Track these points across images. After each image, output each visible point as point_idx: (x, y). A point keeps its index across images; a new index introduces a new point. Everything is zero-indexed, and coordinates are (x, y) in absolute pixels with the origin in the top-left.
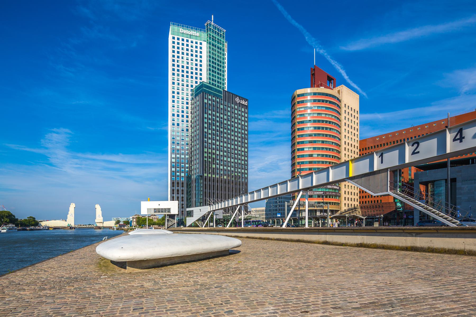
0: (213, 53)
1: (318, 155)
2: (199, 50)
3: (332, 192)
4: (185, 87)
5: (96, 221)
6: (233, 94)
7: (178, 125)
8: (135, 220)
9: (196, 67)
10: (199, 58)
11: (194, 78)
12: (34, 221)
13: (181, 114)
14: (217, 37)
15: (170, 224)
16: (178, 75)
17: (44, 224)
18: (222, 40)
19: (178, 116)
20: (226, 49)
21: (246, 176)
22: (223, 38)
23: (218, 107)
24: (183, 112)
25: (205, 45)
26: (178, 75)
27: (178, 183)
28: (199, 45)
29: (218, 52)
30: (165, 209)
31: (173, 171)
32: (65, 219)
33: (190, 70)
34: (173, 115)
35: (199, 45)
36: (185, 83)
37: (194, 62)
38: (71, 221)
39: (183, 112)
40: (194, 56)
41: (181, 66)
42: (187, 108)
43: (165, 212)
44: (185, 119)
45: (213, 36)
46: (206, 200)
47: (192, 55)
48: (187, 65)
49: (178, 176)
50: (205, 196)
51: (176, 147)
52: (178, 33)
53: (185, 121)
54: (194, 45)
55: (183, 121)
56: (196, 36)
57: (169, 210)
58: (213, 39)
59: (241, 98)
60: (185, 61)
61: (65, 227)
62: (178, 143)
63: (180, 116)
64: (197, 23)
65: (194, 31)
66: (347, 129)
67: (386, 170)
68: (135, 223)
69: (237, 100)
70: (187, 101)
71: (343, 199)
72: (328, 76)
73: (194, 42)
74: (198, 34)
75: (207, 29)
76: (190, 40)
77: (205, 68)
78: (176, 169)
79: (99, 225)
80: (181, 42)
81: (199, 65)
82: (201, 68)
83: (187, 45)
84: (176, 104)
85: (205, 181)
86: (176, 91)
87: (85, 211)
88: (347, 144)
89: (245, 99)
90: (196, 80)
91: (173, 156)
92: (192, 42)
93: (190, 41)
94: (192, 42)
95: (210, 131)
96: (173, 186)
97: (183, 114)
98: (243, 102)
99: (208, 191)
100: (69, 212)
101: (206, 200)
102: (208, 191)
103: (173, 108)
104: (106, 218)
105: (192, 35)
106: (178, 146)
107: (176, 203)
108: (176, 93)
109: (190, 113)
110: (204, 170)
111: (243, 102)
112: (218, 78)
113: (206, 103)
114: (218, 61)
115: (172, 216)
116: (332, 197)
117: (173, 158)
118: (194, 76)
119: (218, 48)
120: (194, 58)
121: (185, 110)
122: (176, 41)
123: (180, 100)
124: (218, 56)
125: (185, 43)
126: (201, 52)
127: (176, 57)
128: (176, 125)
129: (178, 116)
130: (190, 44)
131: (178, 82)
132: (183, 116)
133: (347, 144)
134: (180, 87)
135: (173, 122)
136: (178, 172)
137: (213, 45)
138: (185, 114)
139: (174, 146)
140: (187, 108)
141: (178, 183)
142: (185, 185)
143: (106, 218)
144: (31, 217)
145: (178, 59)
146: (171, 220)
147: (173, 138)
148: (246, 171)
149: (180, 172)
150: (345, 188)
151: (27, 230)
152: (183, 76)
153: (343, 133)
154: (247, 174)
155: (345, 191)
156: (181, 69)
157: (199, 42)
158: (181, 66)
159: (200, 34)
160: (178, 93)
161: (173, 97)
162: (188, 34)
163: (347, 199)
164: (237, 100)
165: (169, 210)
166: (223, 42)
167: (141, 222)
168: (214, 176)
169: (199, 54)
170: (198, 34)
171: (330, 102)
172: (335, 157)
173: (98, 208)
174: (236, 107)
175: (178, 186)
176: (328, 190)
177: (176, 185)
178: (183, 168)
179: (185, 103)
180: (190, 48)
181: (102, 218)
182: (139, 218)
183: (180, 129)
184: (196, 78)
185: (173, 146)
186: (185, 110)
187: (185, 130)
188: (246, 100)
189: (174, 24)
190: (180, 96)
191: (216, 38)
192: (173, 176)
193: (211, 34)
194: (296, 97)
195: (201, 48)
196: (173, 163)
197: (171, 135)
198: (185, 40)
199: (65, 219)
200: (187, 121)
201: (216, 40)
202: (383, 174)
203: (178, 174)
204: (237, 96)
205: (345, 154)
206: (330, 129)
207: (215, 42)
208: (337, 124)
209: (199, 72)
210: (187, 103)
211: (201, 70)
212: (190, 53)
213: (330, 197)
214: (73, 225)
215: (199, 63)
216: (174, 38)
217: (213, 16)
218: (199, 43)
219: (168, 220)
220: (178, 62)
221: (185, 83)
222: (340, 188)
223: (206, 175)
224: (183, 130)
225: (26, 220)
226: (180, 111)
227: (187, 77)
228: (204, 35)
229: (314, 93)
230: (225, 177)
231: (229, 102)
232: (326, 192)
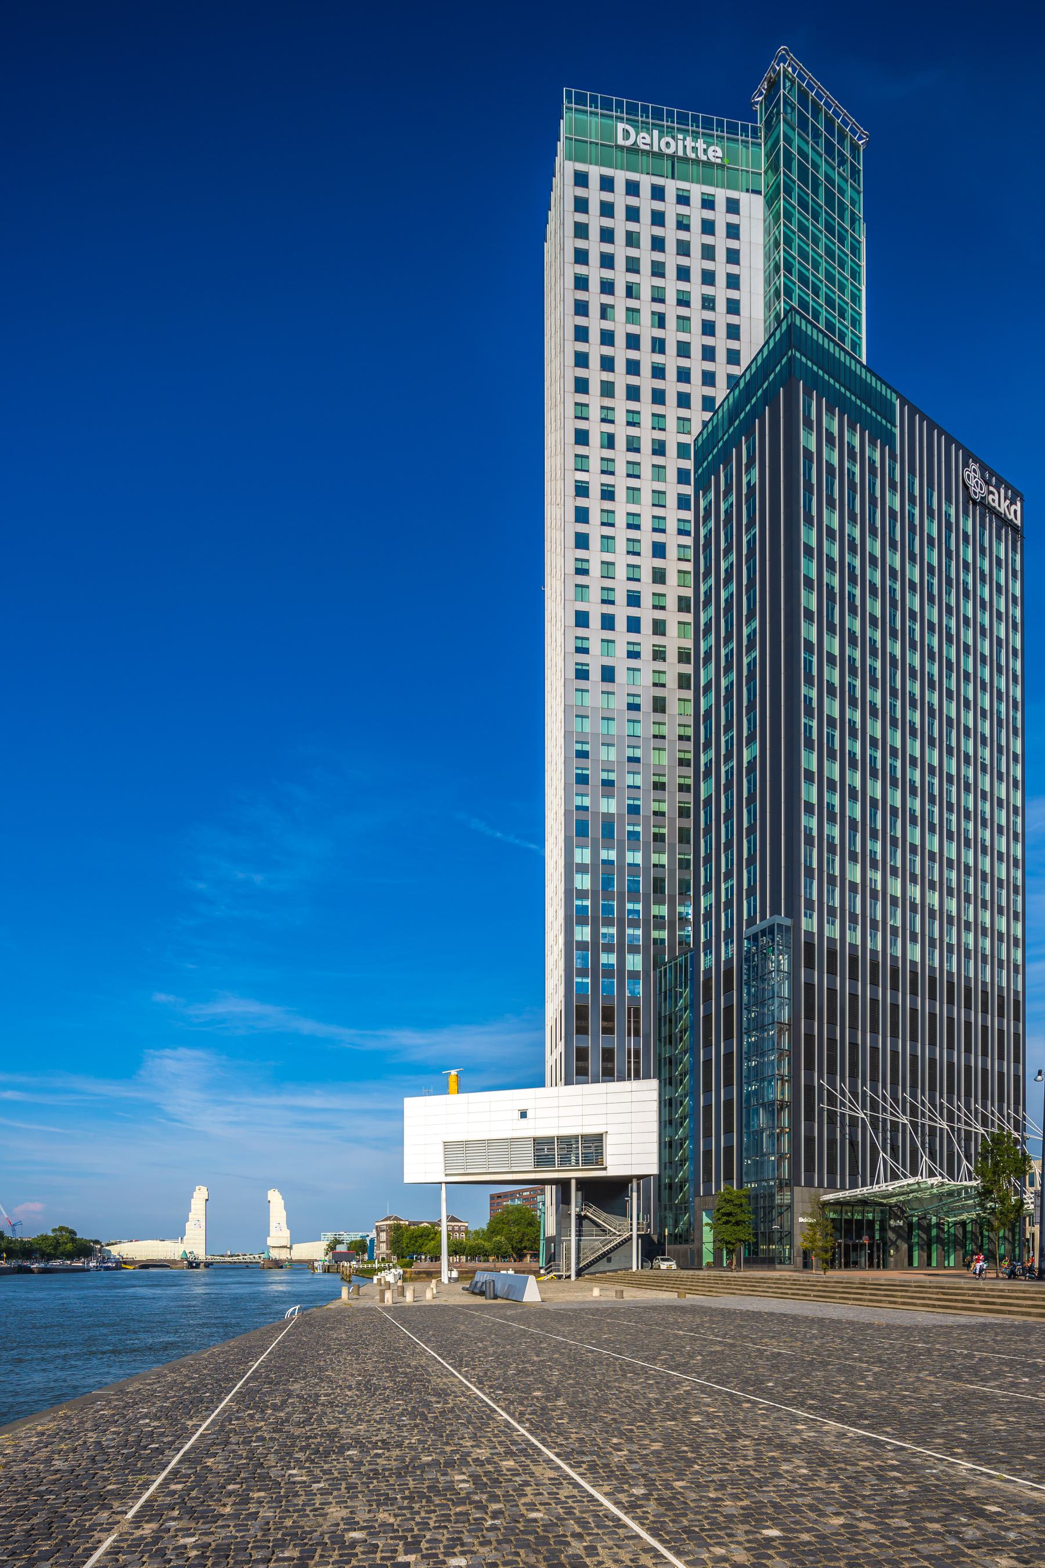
2: (721, 242)
4: (646, 459)
5: (270, 1242)
7: (608, 674)
8: (383, 1236)
9: (709, 341)
10: (721, 293)
12: (73, 1240)
13: (621, 612)
15: (595, 1244)
16: (607, 389)
17: (115, 1251)
19: (608, 622)
24: (634, 599)
26: (607, 389)
27: (608, 1014)
28: (721, 217)
30: (567, 1142)
31: (582, 946)
32: (178, 1233)
33: (671, 361)
34: (582, 619)
35: (721, 217)
36: (646, 435)
37: (697, 314)
38: (194, 1243)
39: (634, 599)
40: (696, 276)
41: (620, 340)
42: (659, 576)
43: (565, 1160)
44: (646, 640)
46: (809, 1088)
47: (683, 274)
48: (659, 333)
49: (608, 971)
50: (809, 1067)
52: (609, 152)
53: (647, 653)
54: (696, 214)
55: (634, 655)
56: (708, 164)
60: (646, 306)
61: (174, 1262)
62: (608, 784)
63: (621, 624)
64: (718, 100)
65: (696, 136)
68: (383, 1246)
70: (659, 537)
73: (696, 200)
74: (715, 153)
76: (671, 187)
78: (595, 933)
79: (275, 1254)
80: (620, 199)
83: (658, 218)
84: (595, 556)
86: (595, 480)
87: (236, 1214)
91: (583, 856)
93: (671, 195)
94: (683, 199)
95: (833, 644)
96: (582, 1030)
97: (634, 612)
100: (191, 1215)
101: (809, 1088)
103: (581, 580)
104: (298, 1236)
105: (685, 160)
106: (608, 796)
107: (644, 1094)
108: (595, 491)
109: (672, 603)
115: (608, 1193)
117: (582, 869)
120: (696, 289)
121: (646, 588)
122: (595, 195)
123: (621, 533)
125: (646, 204)
127: (594, 285)
128: (595, 674)
129: (608, 622)
130: (671, 209)
131: (607, 428)
132: (634, 625)
134: (621, 455)
135: (582, 658)
136: (608, 949)
138: (646, 614)
139: (587, 802)
140: (659, 576)
141: (608, 1014)
142: (648, 1023)
143: (298, 1236)
144: (62, 1229)
145: (607, 299)
146: (601, 1217)
147: (582, 755)
149: (622, 948)
151: (30, 1271)
152: (633, 393)
156: (621, 354)
157: (721, 195)
158: (620, 340)
159: (728, 153)
160: (608, 494)
161: (582, 515)
162: (660, 155)
167: (405, 1241)
169: (721, 268)
170: (715, 153)
173: (276, 1199)
175: (608, 1031)
177: (595, 1021)
178: (634, 924)
179: (646, 549)
180: (671, 234)
181: (287, 1233)
182: (397, 1228)
183: (618, 703)
185: (578, 801)
186: (646, 588)
187: (646, 705)
189: (581, 100)
190: (621, 507)
192: (582, 973)
195: (733, 231)
196: (582, 894)
197: (567, 734)
198: (645, 191)
199: (178, 1233)
200: (659, 655)
203: (608, 959)
210: (659, 550)
212: (671, 260)
214: (200, 1253)
215: (721, 317)
216: (581, 179)
218: (721, 204)
219: (580, 1218)
220: (603, 316)
221: (646, 435)
224: (634, 707)
225: (45, 1238)
226: (621, 598)
227: (659, 397)
228: (753, 157)
230: (915, 953)
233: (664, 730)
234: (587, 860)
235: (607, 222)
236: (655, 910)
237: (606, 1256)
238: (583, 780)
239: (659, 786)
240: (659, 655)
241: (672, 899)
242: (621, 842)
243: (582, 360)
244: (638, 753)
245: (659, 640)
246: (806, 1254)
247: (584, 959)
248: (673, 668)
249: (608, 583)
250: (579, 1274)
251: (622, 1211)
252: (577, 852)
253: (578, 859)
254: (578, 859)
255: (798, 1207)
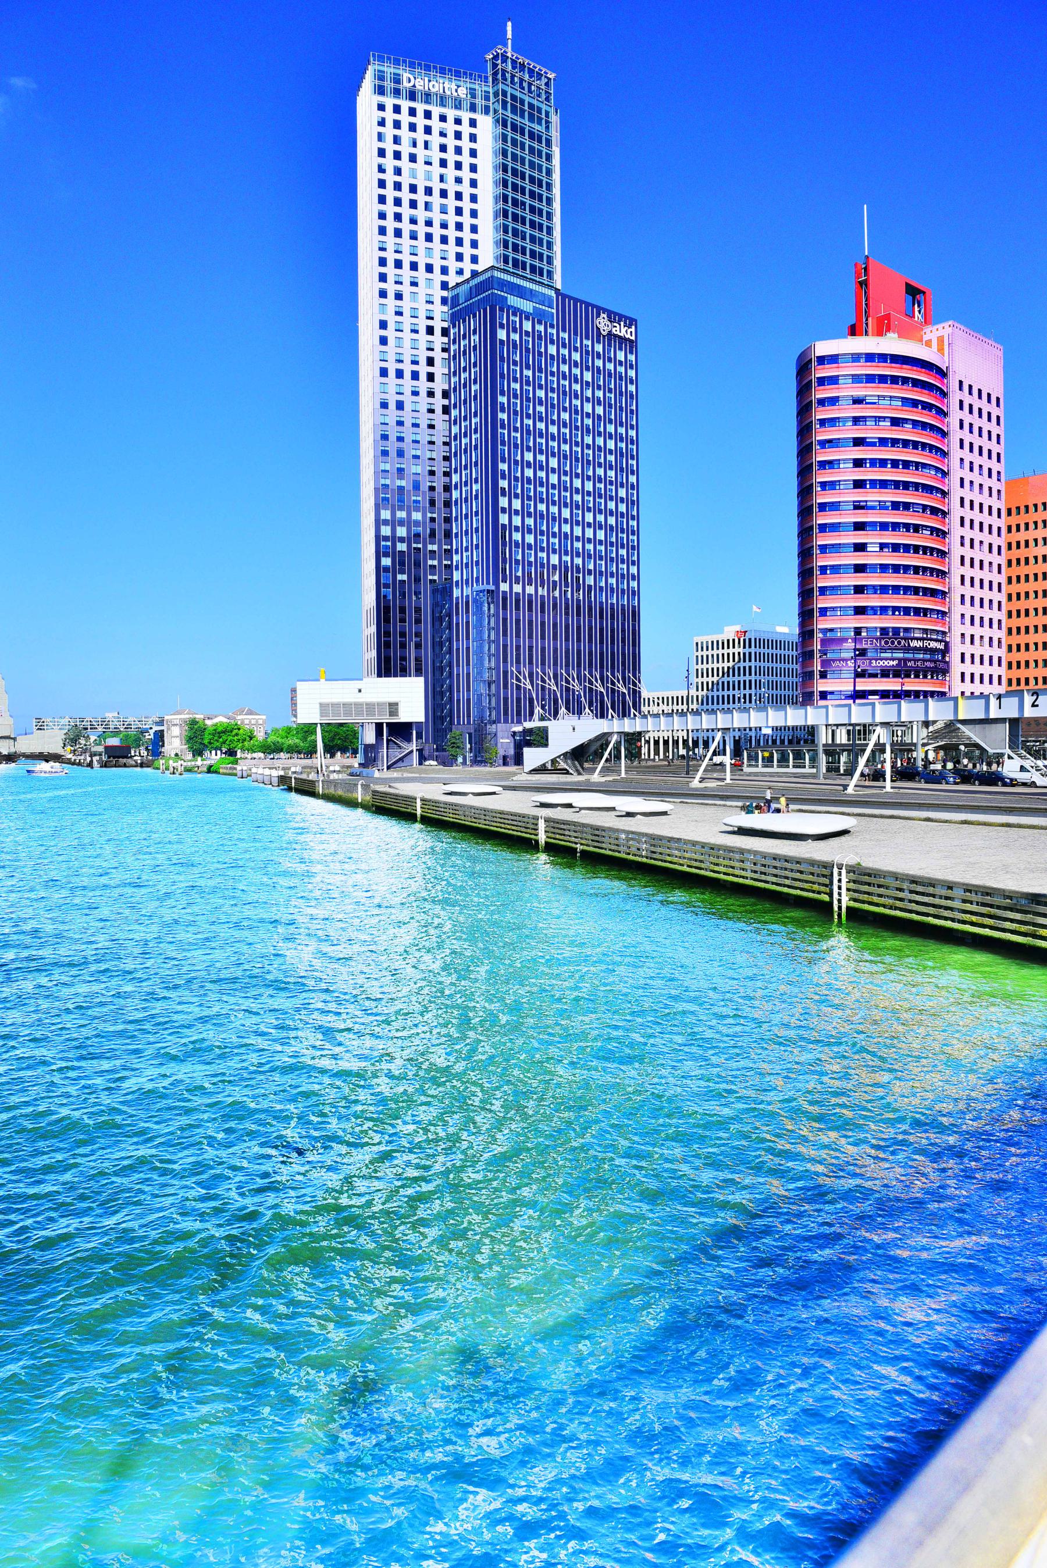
0: (514, 157)
1: (882, 546)
2: (466, 144)
3: (924, 660)
6: (588, 304)
10: (466, 174)
11: (452, 241)
14: (527, 99)
18: (544, 107)
20: (555, 134)
21: (634, 584)
22: (547, 99)
23: (540, 354)
25: (486, 125)
28: (466, 129)
29: (532, 150)
35: (466, 129)
44: (423, 385)
45: (514, 98)
46: (505, 673)
51: (393, 482)
53: (423, 393)
54: (450, 127)
55: (415, 393)
57: (393, 708)
58: (514, 110)
59: (614, 317)
63: (407, 375)
66: (968, 457)
67: (1002, 720)
69: (603, 323)
71: (956, 581)
72: (908, 285)
73: (451, 119)
75: (495, 74)
77: (487, 206)
81: (466, 197)
82: (474, 206)
85: (505, 608)
88: (967, 504)
89: (626, 318)
90: (459, 249)
92: (443, 118)
93: (435, 116)
94: (443, 118)
98: (621, 330)
99: (511, 641)
101: (505, 673)
102: (511, 641)
110: (498, 574)
111: (621, 330)
112: (533, 239)
113: (502, 342)
114: (532, 180)
115: (401, 731)
116: (925, 677)
117: (386, 522)
118: (452, 233)
119: (532, 136)
124: (532, 165)
126: (473, 153)
130: (435, 124)
133: (967, 504)
137: (514, 127)
139: (388, 482)
148: (634, 570)
150: (963, 643)
153: (957, 473)
154: (636, 578)
155: (963, 655)
163: (968, 678)
164: (603, 323)
165: (393, 708)
166: (547, 114)
168: (530, 590)
169: (466, 160)
171: (916, 383)
172: (932, 549)
174: (599, 348)
176: (910, 656)
184: (459, 242)
185: (383, 481)
188: (631, 322)
191: (522, 102)
192: (386, 586)
193: (509, 91)
194: (814, 363)
195: (473, 138)
200: (431, 394)
201: (523, 111)
202: (1000, 726)
204: (600, 310)
205: (962, 460)
206: (917, 464)
207: (522, 116)
208: (938, 449)
209: (467, 220)
210: (430, 362)
211: (474, 214)
213: (917, 676)
217: (509, 24)
222: (947, 644)
223: (504, 587)
229: (867, 355)
231: (576, 334)
232: (906, 660)
233: (434, 439)
234: (389, 517)
235: (398, 194)
236: (430, 547)
237: (401, 759)
238: (385, 453)
239: (432, 473)
240: (431, 394)
241: (440, 541)
242: (409, 507)
243: (382, 199)
244: (418, 453)
245: (430, 385)
246: (505, 758)
247: (387, 578)
248: (439, 402)
249: (399, 350)
250: (388, 768)
251: (409, 740)
252: (383, 512)
253: (383, 517)
254: (383, 517)
255: (499, 734)
